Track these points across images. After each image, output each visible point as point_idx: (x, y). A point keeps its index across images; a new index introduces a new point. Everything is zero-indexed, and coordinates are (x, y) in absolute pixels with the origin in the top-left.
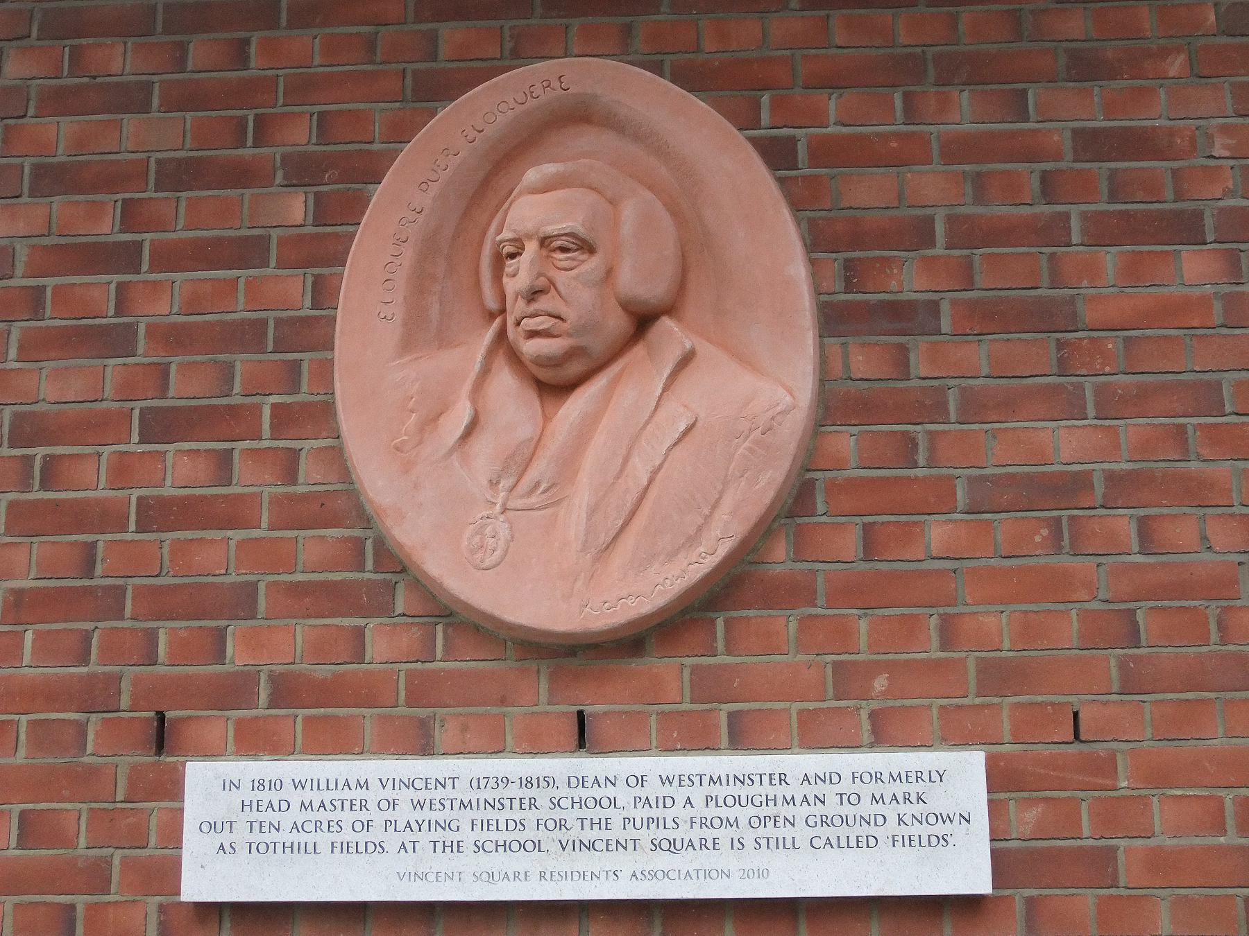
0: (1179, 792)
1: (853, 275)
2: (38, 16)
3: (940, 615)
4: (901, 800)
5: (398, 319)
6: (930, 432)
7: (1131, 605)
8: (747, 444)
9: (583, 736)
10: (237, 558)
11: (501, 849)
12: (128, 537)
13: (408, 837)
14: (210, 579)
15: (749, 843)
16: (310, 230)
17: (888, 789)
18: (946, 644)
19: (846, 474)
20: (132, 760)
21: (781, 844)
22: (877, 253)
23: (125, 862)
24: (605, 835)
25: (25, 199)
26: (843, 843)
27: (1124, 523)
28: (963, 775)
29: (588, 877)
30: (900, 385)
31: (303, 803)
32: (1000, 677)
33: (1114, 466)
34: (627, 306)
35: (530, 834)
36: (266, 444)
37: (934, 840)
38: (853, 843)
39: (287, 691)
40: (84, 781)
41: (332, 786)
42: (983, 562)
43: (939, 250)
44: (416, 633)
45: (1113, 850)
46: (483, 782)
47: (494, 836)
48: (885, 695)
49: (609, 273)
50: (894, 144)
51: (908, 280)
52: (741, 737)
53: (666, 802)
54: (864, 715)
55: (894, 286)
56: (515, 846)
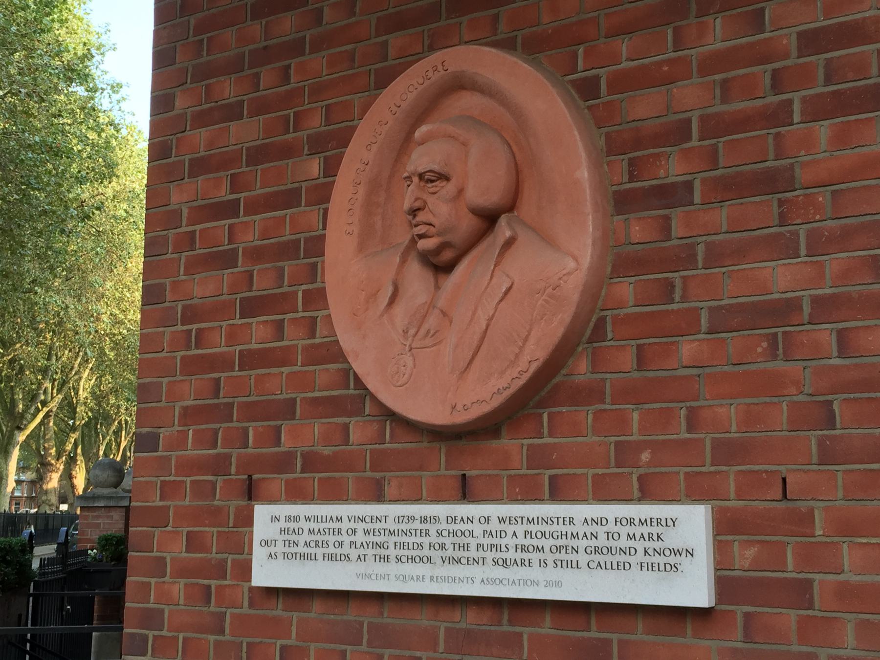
0: (864, 540)
1: (635, 170)
2: (190, 69)
3: (687, 408)
4: (647, 538)
5: (356, 232)
6: (683, 277)
7: (830, 397)
8: (544, 297)
9: (466, 492)
10: (286, 384)
11: (410, 561)
12: (235, 374)
13: (362, 552)
14: (274, 397)
15: (550, 563)
16: (322, 180)
17: (638, 530)
18: (690, 429)
19: (625, 311)
20: (235, 504)
21: (570, 564)
22: (652, 151)
23: (233, 560)
24: (466, 554)
25: (186, 180)
26: (609, 566)
27: (826, 334)
28: (691, 524)
29: (457, 581)
30: (664, 244)
31: (692, 555)
32: (729, 452)
33: (820, 292)
34: (476, 212)
35: (426, 552)
36: (301, 314)
37: (668, 567)
38: (615, 566)
39: (311, 462)
40: (216, 515)
41: (324, 520)
42: (718, 369)
43: (694, 143)
44: (375, 426)
45: (810, 582)
46: (401, 519)
47: (406, 552)
48: (649, 464)
49: (461, 191)
50: (666, 68)
51: (673, 168)
52: (558, 492)
53: (501, 534)
54: (635, 478)
55: (662, 173)
56: (417, 559)
